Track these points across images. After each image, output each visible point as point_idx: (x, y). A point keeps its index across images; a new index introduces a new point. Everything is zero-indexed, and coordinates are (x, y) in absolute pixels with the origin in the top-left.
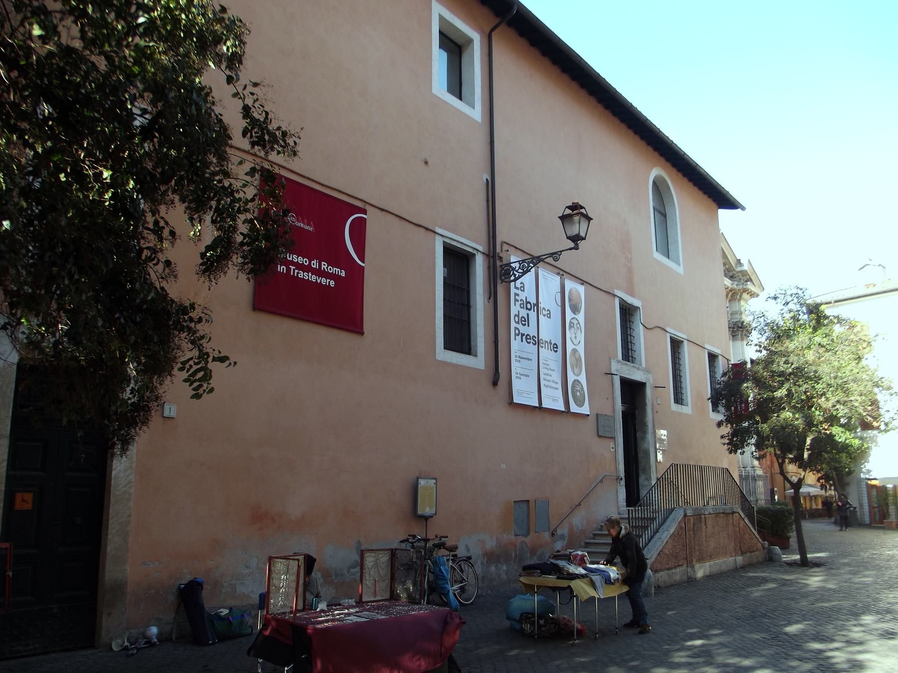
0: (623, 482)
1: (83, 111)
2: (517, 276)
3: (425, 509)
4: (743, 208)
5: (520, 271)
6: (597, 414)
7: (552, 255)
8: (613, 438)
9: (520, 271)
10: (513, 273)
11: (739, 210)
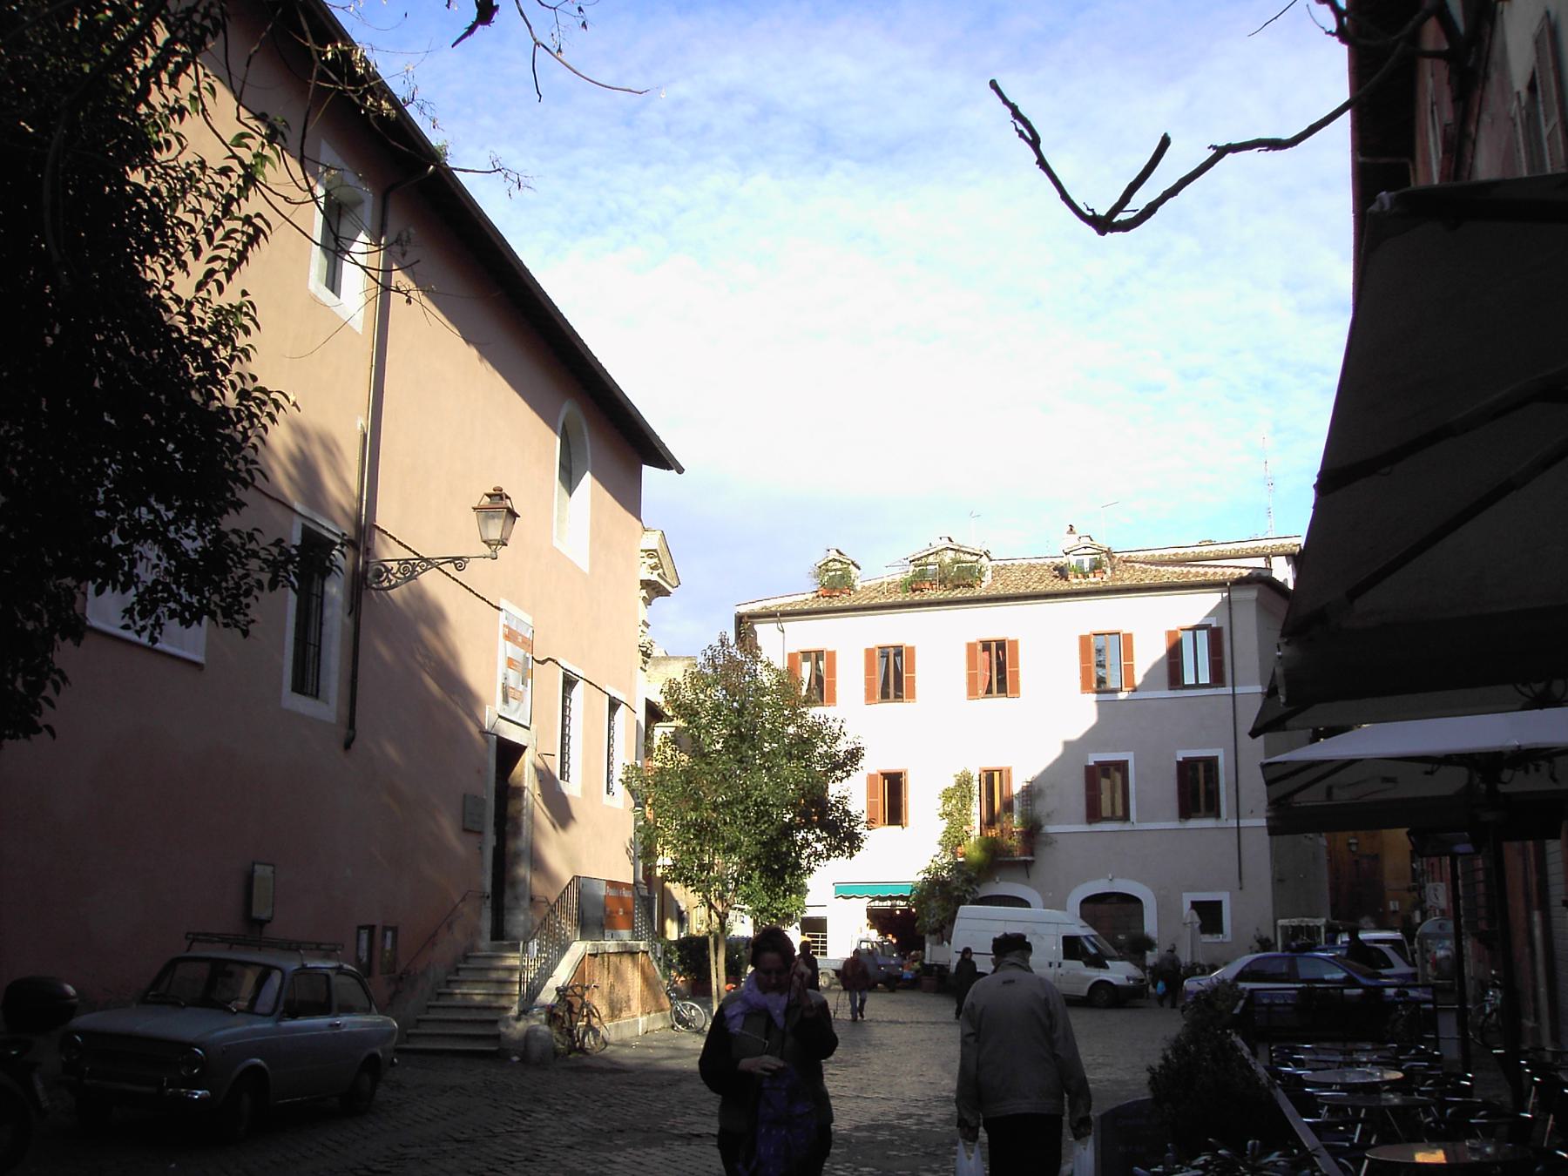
0: (489, 903)
1: (130, 347)
2: (393, 583)
3: (260, 911)
4: (680, 470)
5: (398, 575)
6: (465, 796)
7: (453, 560)
8: (480, 833)
9: (398, 575)
10: (387, 576)
11: (674, 471)
